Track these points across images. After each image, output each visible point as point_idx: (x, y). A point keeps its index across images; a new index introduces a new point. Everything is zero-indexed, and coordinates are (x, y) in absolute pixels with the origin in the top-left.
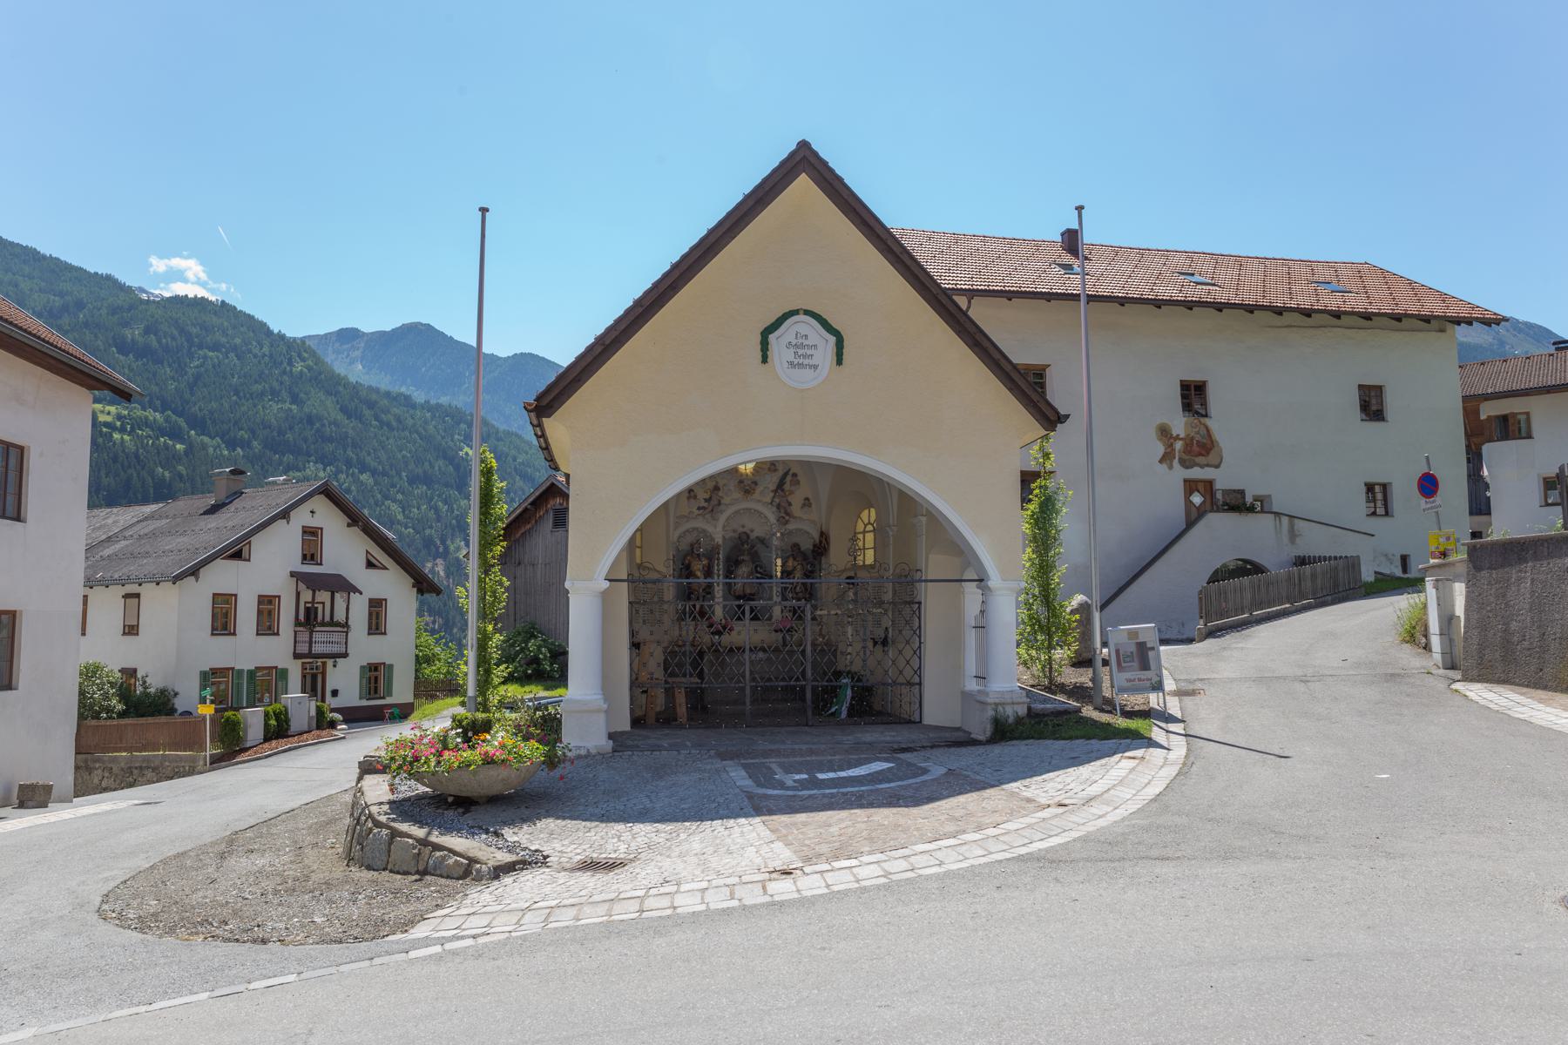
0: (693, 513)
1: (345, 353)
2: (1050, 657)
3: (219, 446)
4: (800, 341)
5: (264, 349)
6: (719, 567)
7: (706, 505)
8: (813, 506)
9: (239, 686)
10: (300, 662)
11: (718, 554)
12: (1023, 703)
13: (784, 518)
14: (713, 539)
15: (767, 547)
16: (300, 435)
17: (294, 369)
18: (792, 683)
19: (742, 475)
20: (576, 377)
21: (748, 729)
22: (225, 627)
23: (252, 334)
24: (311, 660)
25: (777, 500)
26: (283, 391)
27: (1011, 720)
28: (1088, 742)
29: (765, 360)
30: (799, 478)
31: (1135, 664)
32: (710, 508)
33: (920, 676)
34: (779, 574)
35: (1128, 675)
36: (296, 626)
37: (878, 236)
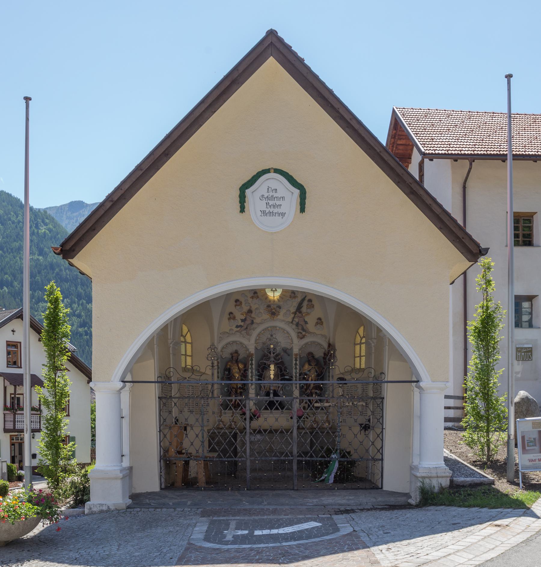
0: (233, 330)
1: (75, 219)
2: (488, 440)
4: (271, 194)
5: (19, 218)
6: (252, 372)
7: (242, 324)
8: (324, 323)
10: (8, 435)
11: (252, 360)
12: (447, 477)
13: (301, 333)
14: (247, 350)
15: (289, 355)
16: (45, 277)
17: (40, 231)
18: (282, 458)
19: (270, 301)
21: (248, 491)
24: (16, 434)
25: (296, 320)
27: (436, 490)
28: (481, 510)
29: (242, 209)
30: (313, 303)
31: (537, 448)
32: (245, 327)
33: (382, 454)
34: (272, 377)
35: (531, 456)
36: (4, 410)
37: (332, 106)
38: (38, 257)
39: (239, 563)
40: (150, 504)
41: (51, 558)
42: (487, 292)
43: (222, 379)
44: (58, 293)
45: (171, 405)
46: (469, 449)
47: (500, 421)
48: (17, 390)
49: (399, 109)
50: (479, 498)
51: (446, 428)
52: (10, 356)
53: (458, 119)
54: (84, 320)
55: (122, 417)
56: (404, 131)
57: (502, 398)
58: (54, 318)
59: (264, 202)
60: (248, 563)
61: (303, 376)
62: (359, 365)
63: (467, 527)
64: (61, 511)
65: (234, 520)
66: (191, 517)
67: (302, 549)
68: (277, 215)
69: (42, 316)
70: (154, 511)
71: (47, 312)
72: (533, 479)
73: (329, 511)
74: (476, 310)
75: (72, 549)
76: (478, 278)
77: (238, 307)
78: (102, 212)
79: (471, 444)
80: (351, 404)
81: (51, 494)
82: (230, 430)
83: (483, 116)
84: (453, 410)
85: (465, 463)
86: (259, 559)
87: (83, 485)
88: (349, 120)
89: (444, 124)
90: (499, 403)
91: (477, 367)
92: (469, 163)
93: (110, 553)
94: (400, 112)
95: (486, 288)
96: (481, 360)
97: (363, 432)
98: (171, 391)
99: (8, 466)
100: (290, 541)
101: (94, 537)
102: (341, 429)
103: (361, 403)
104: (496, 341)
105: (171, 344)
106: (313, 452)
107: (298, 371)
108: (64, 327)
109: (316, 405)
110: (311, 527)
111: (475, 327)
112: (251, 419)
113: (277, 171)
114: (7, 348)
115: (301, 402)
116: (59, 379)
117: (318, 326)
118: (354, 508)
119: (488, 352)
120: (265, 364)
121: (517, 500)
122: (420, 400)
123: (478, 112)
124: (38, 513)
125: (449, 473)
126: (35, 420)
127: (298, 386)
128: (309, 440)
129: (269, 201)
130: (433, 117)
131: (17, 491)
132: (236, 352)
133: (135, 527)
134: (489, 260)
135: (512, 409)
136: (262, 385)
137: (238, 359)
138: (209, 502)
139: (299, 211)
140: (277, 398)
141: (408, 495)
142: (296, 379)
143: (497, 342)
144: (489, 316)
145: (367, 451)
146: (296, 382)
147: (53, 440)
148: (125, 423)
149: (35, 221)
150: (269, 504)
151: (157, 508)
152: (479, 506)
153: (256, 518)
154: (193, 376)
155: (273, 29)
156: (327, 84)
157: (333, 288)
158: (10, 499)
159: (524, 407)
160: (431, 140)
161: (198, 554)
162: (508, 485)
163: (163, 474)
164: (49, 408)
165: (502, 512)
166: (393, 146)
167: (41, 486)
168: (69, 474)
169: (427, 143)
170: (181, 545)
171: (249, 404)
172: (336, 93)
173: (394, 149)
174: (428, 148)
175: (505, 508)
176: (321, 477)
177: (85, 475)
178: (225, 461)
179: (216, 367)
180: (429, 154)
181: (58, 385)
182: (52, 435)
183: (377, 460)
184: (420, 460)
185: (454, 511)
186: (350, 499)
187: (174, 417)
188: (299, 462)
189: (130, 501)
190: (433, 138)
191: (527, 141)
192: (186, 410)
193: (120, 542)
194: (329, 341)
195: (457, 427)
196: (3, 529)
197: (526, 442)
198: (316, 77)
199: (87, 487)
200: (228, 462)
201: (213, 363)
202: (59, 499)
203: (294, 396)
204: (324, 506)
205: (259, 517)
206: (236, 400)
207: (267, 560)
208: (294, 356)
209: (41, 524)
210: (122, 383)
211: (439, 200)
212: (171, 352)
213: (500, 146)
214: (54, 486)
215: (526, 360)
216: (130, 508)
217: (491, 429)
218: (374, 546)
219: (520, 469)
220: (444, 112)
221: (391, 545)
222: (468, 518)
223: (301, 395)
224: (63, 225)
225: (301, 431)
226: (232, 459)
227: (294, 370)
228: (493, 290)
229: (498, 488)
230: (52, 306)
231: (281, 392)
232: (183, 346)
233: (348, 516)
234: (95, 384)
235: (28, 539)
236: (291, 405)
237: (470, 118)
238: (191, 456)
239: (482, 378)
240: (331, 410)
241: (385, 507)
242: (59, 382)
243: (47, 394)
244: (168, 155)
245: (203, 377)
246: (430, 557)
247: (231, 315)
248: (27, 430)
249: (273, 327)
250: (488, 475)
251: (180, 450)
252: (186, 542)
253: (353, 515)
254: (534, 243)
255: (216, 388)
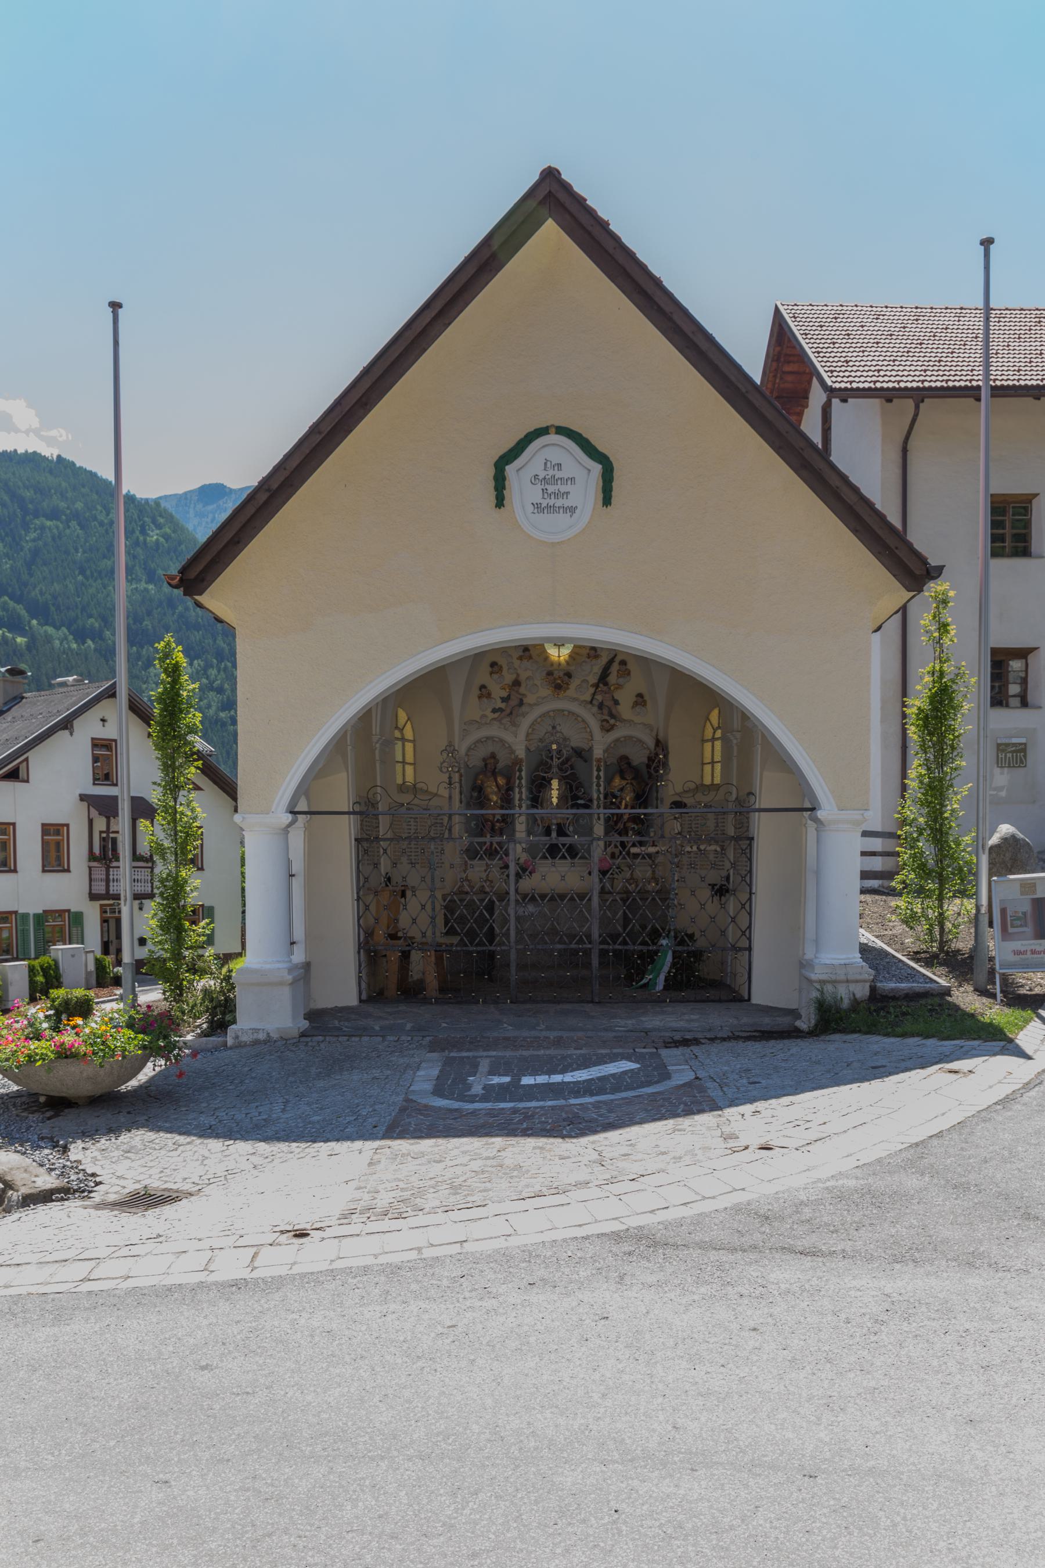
1: (211, 516)
2: (941, 914)
3: (66, 638)
4: (551, 472)
6: (521, 794)
7: (503, 705)
9: (25, 933)
10: (97, 904)
11: (520, 770)
12: (865, 981)
13: (608, 722)
14: (513, 752)
15: (586, 761)
17: (148, 538)
18: (573, 946)
19: (552, 664)
20: (233, 538)
21: (513, 1006)
22: (59, 859)
23: (95, 497)
24: (111, 902)
25: (599, 698)
26: (137, 568)
27: (846, 1004)
28: (924, 1041)
29: (500, 502)
31: (1029, 930)
32: (508, 711)
33: (749, 939)
34: (555, 801)
36: (90, 861)
37: (660, 310)
38: (146, 586)
39: (492, 1136)
40: (339, 1029)
41: (167, 1125)
42: (941, 646)
43: (468, 806)
44: (179, 656)
45: (378, 852)
46: (907, 929)
47: (962, 880)
48: (111, 824)
49: (786, 307)
50: (921, 1020)
51: (864, 891)
52: (99, 764)
53: (895, 322)
54: (228, 697)
55: (292, 876)
56: (794, 347)
57: (967, 838)
58: (173, 700)
59: (539, 487)
60: (508, 1135)
61: (611, 799)
62: (710, 778)
63: (897, 1073)
64: (185, 1043)
65: (486, 1057)
66: (412, 1052)
67: (603, 1111)
68: (561, 511)
69: (154, 692)
70: (348, 1040)
71: (159, 690)
72: (1022, 986)
73: (653, 1042)
74: (922, 678)
75: (204, 1110)
76: (925, 620)
77: (495, 676)
78: (251, 510)
79: (910, 920)
80: (695, 848)
81: (169, 1011)
82: (482, 896)
83: (943, 315)
84: (880, 857)
85: (899, 956)
86: (527, 1129)
87: (224, 994)
88: (691, 335)
89: (869, 333)
90: (962, 847)
91: (921, 782)
92: (913, 405)
93: (270, 1116)
94: (789, 311)
95: (940, 639)
96: (929, 769)
97: (717, 898)
98: (378, 827)
99: (97, 960)
100: (583, 1096)
101: (243, 1088)
102: (677, 894)
103: (713, 847)
104: (957, 734)
105: (377, 743)
106: (627, 935)
107: (602, 789)
108: (190, 716)
109: (634, 850)
110: (621, 1070)
111: (919, 709)
112: (518, 876)
113: (562, 431)
114: (93, 751)
115: (607, 845)
116: (182, 808)
117: (638, 709)
118: (699, 1035)
119: (943, 755)
120: (544, 778)
121: (991, 1024)
122: (818, 842)
123: (932, 308)
124: (144, 1048)
125: (868, 973)
126: (143, 877)
127: (602, 816)
128: (620, 913)
129: (547, 486)
130: (849, 320)
131: (108, 1007)
132: (493, 756)
133: (313, 1070)
134: (946, 586)
135: (984, 859)
136: (537, 816)
137: (495, 768)
138: (444, 1025)
139: (601, 502)
140: (563, 840)
141: (795, 1014)
142: (598, 803)
143: (958, 737)
144: (943, 690)
145: (723, 933)
146: (598, 811)
147: (171, 915)
148: (297, 884)
149: (140, 520)
150: (549, 1028)
151: (353, 1036)
152: (922, 1035)
153: (526, 1053)
154: (416, 801)
155: (552, 166)
156: (651, 268)
157: (661, 641)
158: (96, 1022)
159: (1007, 855)
160: (845, 364)
161: (422, 1120)
162: (976, 997)
163: (363, 975)
164: (164, 860)
165: (962, 1047)
166: (775, 376)
167: (152, 996)
168: (201, 975)
169: (838, 369)
170: (393, 1102)
171: (515, 850)
172: (667, 283)
173: (777, 381)
174: (839, 379)
175: (968, 1039)
176: (641, 980)
177: (228, 978)
178: (472, 952)
179: (457, 785)
180: (840, 389)
181: (181, 818)
182: (170, 907)
183: (741, 949)
184: (817, 951)
185: (877, 1043)
186: (692, 1020)
187: (383, 873)
188: (603, 953)
189: (305, 1024)
190: (849, 359)
191: (1024, 360)
192: (404, 859)
193: (287, 1097)
194: (657, 735)
195: (886, 888)
196: (85, 1074)
197: (1009, 919)
198: (630, 255)
199: (231, 999)
200: (478, 952)
201: (450, 778)
202: (183, 1020)
203: (595, 836)
204: (646, 1033)
205: (531, 1052)
206: (491, 844)
207: (542, 1130)
208: (595, 763)
209: (150, 1065)
210: (290, 817)
211: (853, 479)
212: (377, 757)
213: (972, 370)
214: (174, 998)
215: (1014, 767)
216: (306, 1036)
217: (947, 894)
218: (730, 1106)
219: (997, 967)
220: (870, 309)
221: (760, 1105)
222: (900, 1058)
223: (607, 833)
224: (190, 527)
225: (607, 896)
226: (484, 948)
227: (595, 787)
228: (953, 641)
229: (957, 1002)
230: (169, 679)
231: (571, 829)
232: (399, 745)
233: (687, 1050)
234: (243, 818)
235: (128, 1092)
236: (589, 851)
237: (917, 320)
238: (413, 943)
239: (931, 802)
240: (660, 859)
241: (754, 1034)
242: (182, 813)
243: (161, 835)
244: (366, 404)
245: (434, 802)
246: (828, 1129)
247: (483, 690)
248: (126, 900)
249: (558, 710)
250: (940, 978)
251: (393, 932)
252: (401, 1098)
253: (696, 1049)
254: (1032, 550)
255: (457, 821)
